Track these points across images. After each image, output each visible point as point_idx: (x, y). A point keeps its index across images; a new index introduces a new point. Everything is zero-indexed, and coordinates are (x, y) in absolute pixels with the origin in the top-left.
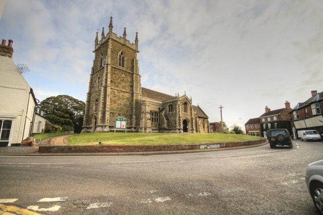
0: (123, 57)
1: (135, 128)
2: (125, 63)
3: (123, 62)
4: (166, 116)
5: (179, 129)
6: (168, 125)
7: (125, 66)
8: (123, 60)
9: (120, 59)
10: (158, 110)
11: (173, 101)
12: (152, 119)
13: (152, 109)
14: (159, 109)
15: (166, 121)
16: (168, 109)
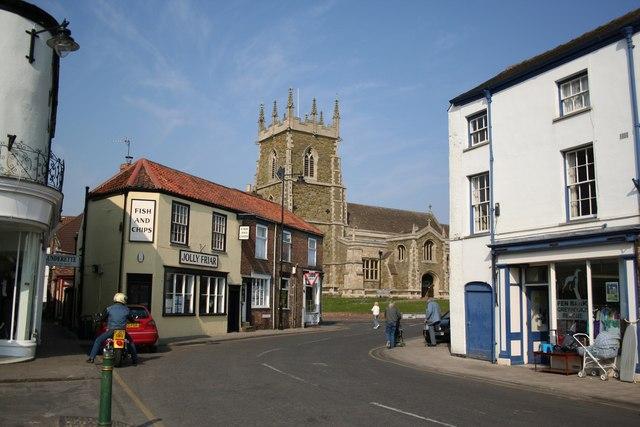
0: (312, 158)
1: (336, 289)
2: (315, 168)
3: (312, 168)
4: (391, 267)
5: (413, 293)
6: (396, 285)
7: (315, 173)
8: (312, 163)
9: (306, 165)
10: (377, 256)
11: (405, 240)
12: (365, 274)
13: (366, 255)
14: (380, 253)
15: (391, 277)
16: (397, 255)
